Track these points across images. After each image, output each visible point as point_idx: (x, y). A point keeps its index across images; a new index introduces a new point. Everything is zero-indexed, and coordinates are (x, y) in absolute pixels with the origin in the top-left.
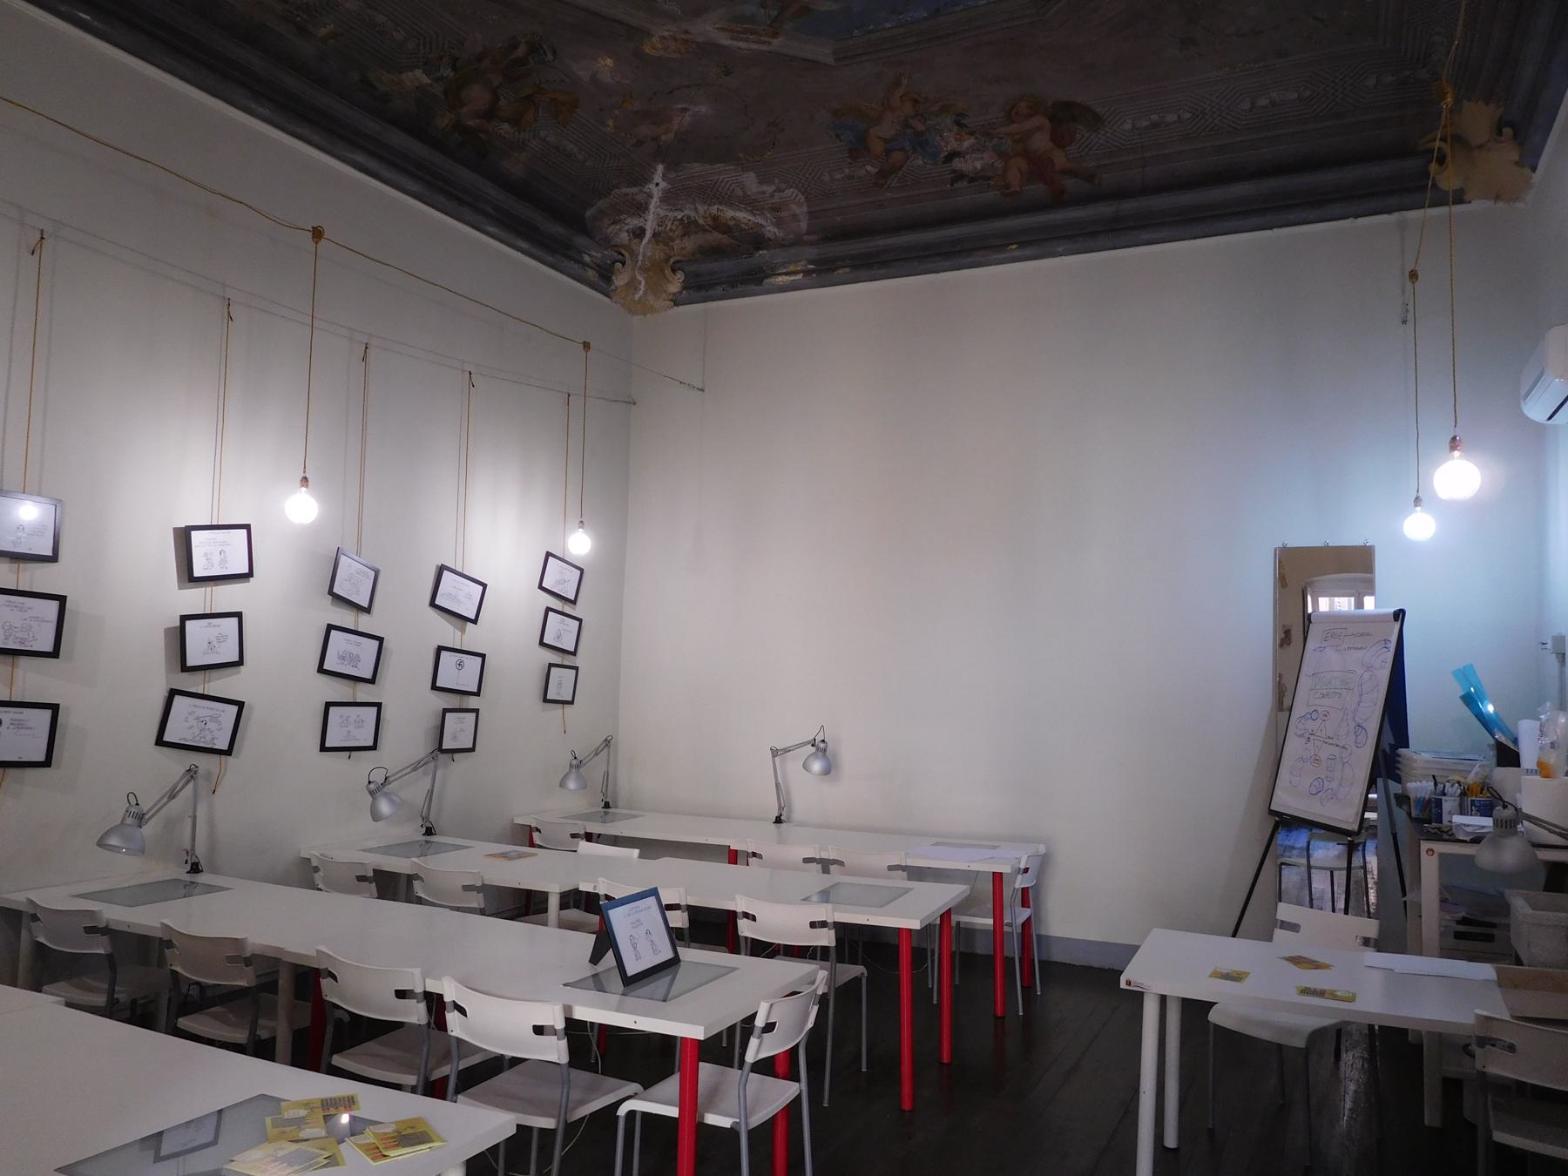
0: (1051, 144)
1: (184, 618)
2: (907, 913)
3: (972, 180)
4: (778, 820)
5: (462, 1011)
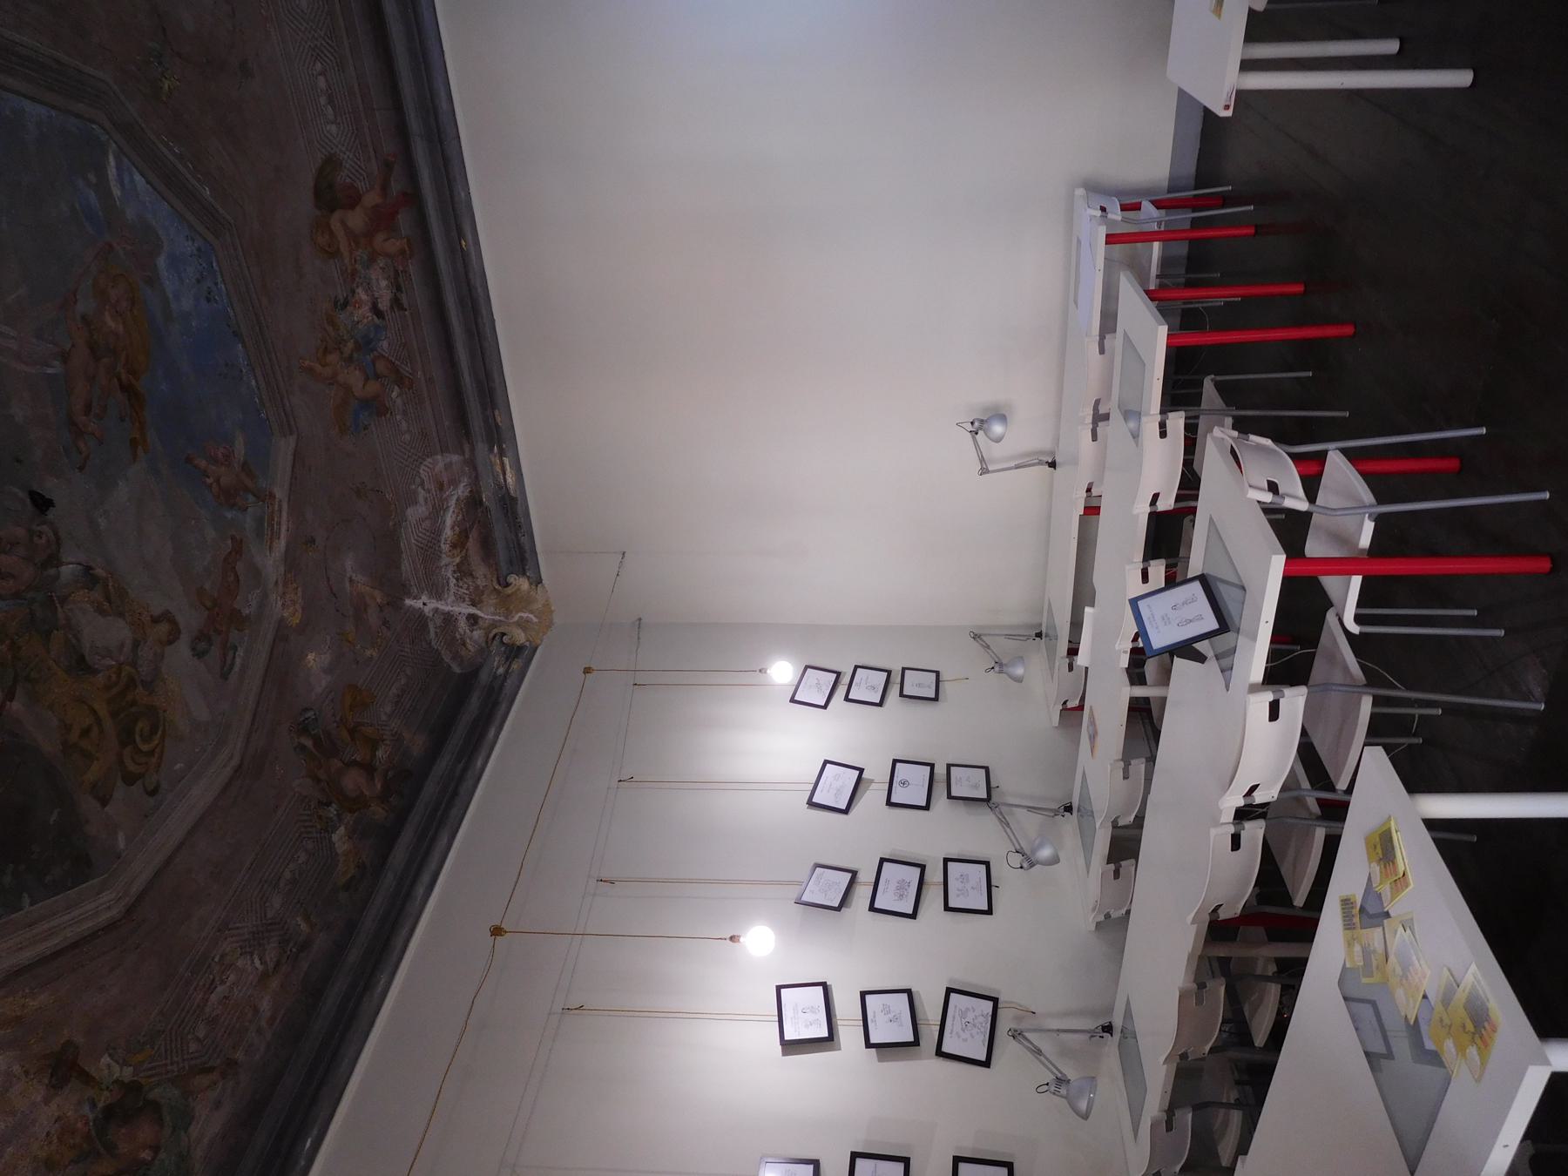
0: (358, 209)
1: (868, 1045)
2: (1152, 338)
3: (399, 289)
4: (1053, 465)
5: (1156, 497)
